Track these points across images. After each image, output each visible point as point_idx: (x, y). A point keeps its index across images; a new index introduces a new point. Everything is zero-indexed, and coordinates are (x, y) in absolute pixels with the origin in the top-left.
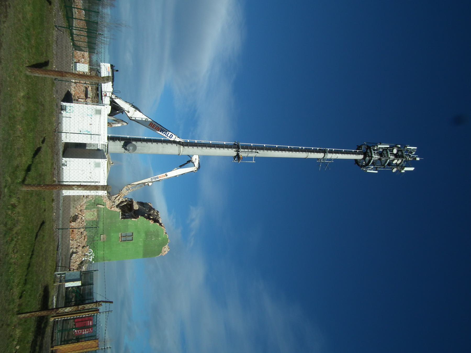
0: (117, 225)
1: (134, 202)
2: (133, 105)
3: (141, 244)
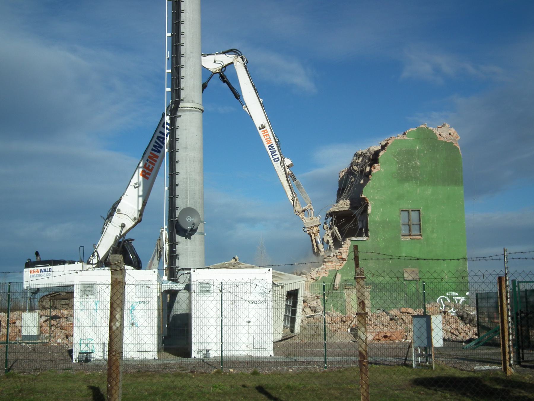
0: (382, 245)
1: (332, 209)
2: (108, 218)
3: (429, 191)
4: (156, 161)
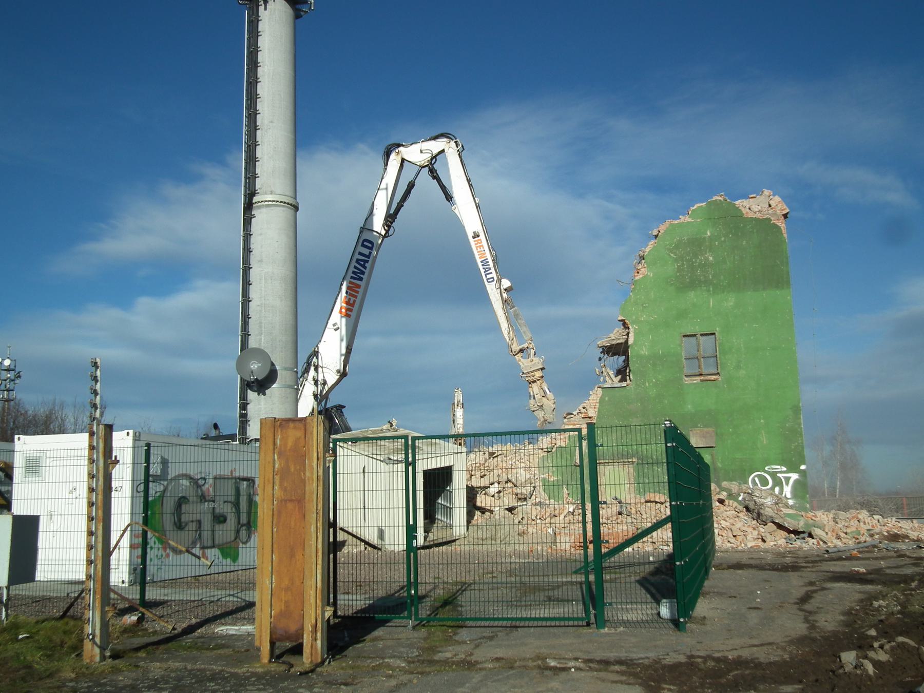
0: (653, 392)
3: (730, 301)
4: (357, 292)
